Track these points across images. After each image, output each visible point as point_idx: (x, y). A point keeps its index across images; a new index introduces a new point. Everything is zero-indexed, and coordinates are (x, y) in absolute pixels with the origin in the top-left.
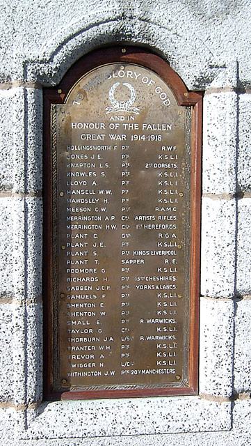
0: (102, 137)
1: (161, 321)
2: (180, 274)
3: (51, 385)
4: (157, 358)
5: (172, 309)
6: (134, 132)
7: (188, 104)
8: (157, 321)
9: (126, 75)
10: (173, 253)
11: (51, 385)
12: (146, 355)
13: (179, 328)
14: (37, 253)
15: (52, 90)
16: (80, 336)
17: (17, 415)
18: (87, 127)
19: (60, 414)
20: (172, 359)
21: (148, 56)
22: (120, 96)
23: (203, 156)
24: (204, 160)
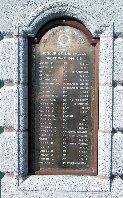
0: (55, 58)
1: (82, 72)
2: (89, 130)
3: (31, 167)
4: (76, 157)
5: (85, 158)
6: (69, 56)
7: (94, 45)
8: (80, 71)
9: (66, 31)
10: (86, 144)
11: (31, 167)
12: (73, 153)
13: (90, 100)
14: (24, 72)
15: (31, 40)
16: (44, 113)
17: (15, 181)
18: (48, 54)
19: (34, 180)
20: (86, 126)
21: (75, 22)
22: (63, 40)
23: (100, 82)
24: (99, 98)
